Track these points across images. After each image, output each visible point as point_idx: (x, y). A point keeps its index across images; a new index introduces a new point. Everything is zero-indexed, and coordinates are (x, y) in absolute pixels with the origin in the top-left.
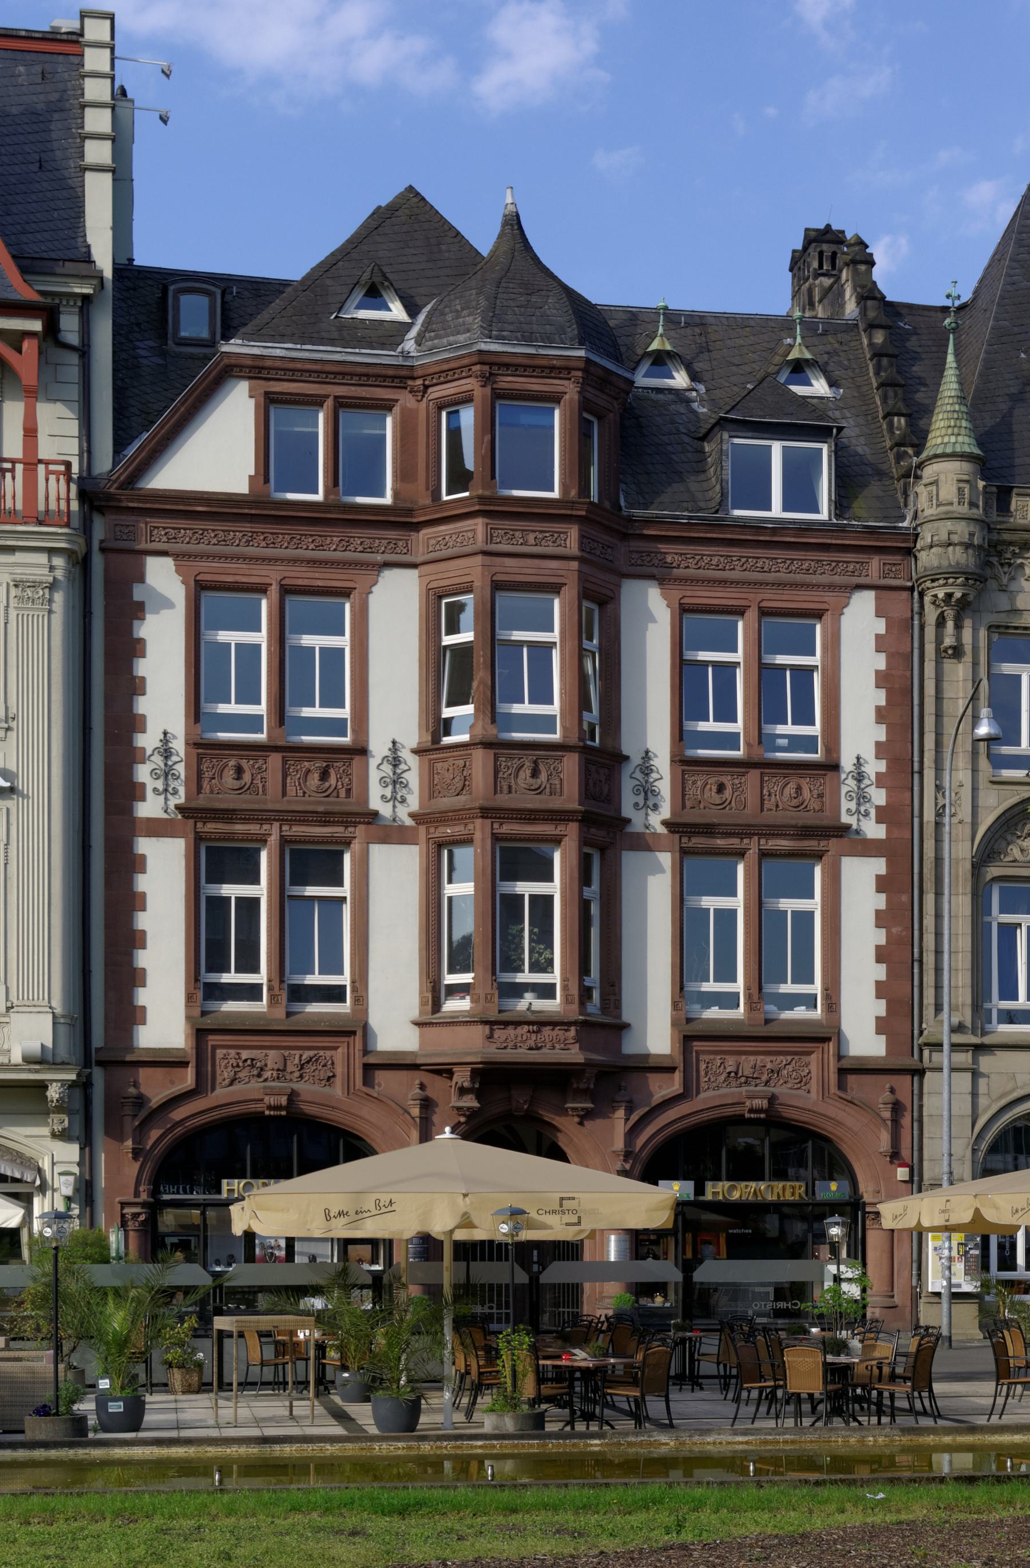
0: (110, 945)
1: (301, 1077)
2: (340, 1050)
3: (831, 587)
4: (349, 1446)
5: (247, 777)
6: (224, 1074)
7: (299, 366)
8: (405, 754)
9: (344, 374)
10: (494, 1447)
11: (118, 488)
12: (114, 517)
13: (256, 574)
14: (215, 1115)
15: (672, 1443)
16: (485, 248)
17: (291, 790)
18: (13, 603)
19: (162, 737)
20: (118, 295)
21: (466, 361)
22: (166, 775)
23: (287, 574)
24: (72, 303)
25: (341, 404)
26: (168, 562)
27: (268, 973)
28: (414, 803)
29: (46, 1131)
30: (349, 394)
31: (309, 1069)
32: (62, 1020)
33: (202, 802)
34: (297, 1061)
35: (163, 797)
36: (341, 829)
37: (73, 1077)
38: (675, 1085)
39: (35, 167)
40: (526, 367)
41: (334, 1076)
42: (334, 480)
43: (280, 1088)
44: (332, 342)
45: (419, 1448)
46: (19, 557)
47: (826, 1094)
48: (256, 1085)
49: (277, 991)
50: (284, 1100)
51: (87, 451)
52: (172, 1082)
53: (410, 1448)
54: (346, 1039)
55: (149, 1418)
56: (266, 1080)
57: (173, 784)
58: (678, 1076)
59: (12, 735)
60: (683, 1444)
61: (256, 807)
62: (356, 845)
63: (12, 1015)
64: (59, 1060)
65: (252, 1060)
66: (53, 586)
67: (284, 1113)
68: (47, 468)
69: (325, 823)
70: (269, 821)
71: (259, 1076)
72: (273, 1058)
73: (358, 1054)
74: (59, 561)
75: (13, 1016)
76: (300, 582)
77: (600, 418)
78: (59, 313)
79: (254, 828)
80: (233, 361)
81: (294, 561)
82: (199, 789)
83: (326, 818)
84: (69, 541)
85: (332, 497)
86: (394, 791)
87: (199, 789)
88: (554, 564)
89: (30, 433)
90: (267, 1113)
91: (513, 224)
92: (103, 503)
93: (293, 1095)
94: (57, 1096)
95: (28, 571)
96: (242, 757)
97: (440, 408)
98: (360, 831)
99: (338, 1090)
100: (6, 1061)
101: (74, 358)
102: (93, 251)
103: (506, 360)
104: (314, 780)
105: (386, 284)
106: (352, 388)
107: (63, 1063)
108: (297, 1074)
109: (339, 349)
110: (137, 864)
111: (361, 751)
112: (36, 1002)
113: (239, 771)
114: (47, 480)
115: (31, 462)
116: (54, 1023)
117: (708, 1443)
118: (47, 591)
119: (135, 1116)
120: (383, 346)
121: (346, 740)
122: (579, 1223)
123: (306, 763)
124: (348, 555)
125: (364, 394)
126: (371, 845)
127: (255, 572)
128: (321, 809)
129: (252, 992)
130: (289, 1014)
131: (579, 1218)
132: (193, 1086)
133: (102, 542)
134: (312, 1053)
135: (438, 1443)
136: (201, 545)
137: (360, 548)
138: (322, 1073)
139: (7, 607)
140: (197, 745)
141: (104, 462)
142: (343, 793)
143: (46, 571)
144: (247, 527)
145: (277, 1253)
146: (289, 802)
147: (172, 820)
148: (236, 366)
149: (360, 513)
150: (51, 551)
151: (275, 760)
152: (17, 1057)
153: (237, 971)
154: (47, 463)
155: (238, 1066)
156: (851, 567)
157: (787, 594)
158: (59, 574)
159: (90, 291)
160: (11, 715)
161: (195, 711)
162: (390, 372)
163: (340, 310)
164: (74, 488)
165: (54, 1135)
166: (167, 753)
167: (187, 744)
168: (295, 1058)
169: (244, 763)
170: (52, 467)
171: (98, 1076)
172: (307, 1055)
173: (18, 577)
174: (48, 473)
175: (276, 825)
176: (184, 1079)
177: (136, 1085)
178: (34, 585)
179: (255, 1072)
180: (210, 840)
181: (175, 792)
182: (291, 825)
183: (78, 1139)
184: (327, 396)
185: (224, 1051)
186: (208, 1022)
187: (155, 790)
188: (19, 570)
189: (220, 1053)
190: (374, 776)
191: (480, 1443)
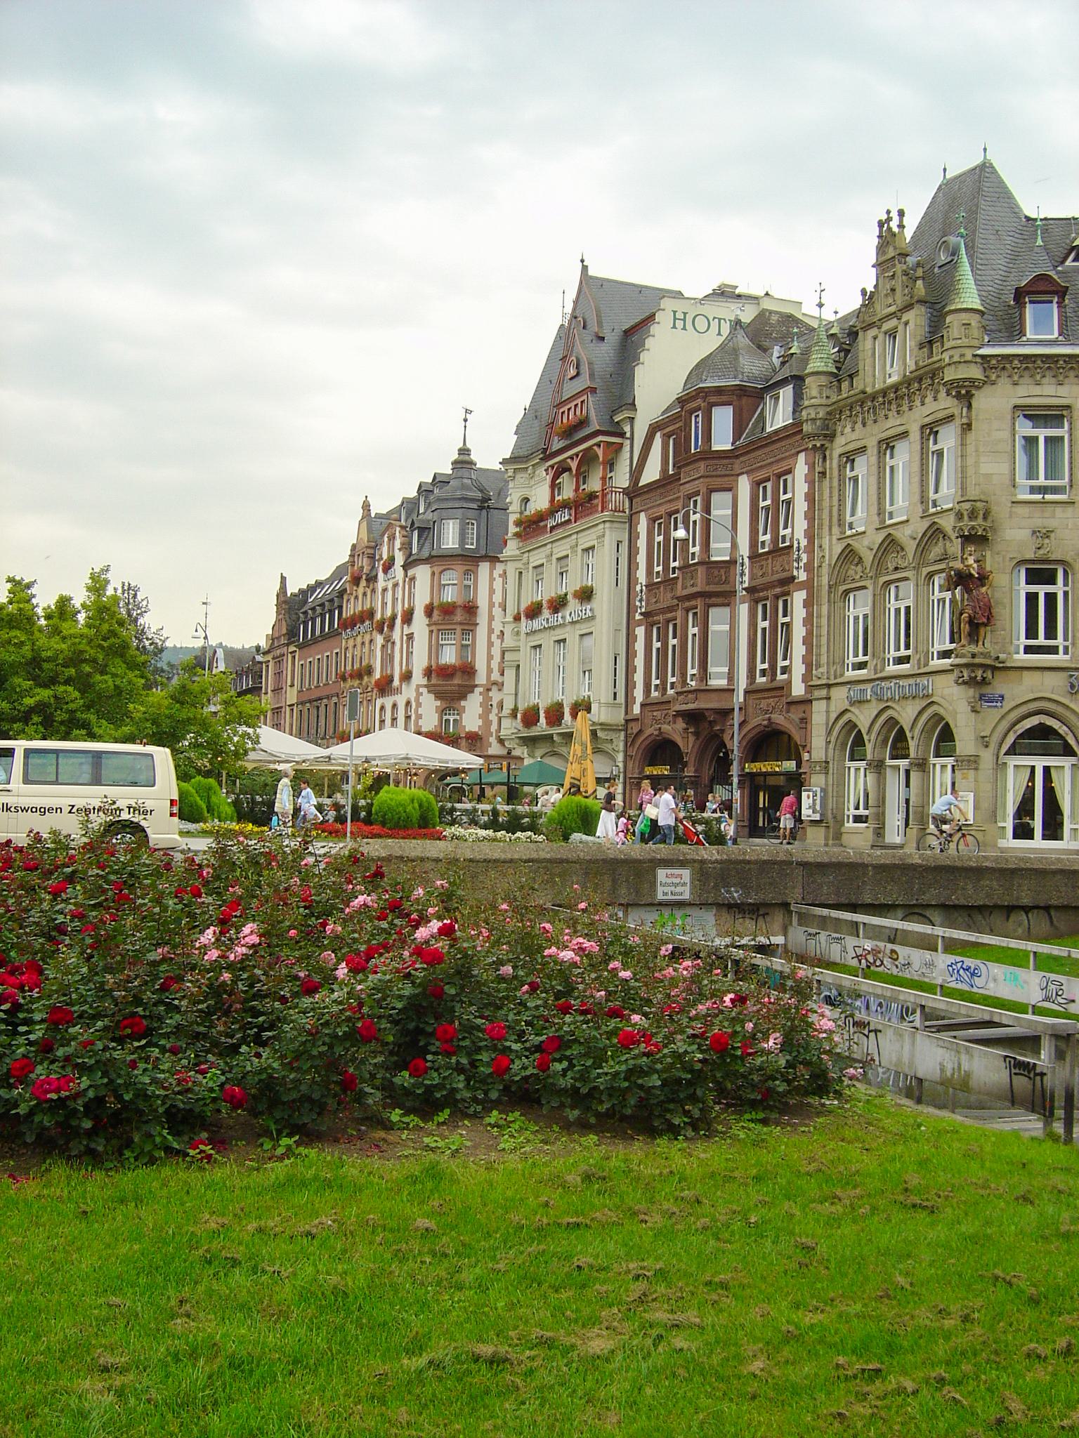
88: (719, 479)
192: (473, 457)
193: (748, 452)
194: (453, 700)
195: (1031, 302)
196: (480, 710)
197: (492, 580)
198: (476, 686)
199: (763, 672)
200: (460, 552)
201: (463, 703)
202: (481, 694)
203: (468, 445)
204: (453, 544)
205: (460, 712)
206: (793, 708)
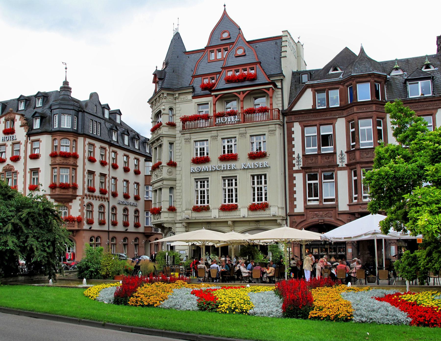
3: (433, 109)
8: (344, 153)
9: (328, 84)
13: (314, 123)
16: (357, 55)
21: (350, 78)
22: (342, 159)
28: (346, 162)
33: (306, 166)
40: (362, 77)
48: (317, 218)
57: (300, 163)
69: (329, 168)
70: (319, 168)
77: (380, 83)
79: (316, 170)
86: (342, 160)
88: (370, 113)
91: (362, 51)
97: (347, 87)
98: (336, 169)
101: (280, 90)
103: (357, 76)
110: (294, 178)
120: (336, 77)
128: (328, 165)
151: (319, 157)
152: (271, 215)
154: (274, 109)
156: (438, 104)
157: (423, 112)
166: (298, 157)
171: (288, 218)
172: (327, 212)
175: (320, 169)
176: (304, 218)
192: (70, 86)
193: (432, 101)
194: (65, 202)
195: (410, 84)
196: (80, 208)
197: (84, 146)
198: (77, 196)
199: (356, 198)
200: (72, 131)
201: (70, 204)
202: (80, 200)
203: (68, 80)
204: (67, 126)
205: (69, 208)
206: (340, 215)
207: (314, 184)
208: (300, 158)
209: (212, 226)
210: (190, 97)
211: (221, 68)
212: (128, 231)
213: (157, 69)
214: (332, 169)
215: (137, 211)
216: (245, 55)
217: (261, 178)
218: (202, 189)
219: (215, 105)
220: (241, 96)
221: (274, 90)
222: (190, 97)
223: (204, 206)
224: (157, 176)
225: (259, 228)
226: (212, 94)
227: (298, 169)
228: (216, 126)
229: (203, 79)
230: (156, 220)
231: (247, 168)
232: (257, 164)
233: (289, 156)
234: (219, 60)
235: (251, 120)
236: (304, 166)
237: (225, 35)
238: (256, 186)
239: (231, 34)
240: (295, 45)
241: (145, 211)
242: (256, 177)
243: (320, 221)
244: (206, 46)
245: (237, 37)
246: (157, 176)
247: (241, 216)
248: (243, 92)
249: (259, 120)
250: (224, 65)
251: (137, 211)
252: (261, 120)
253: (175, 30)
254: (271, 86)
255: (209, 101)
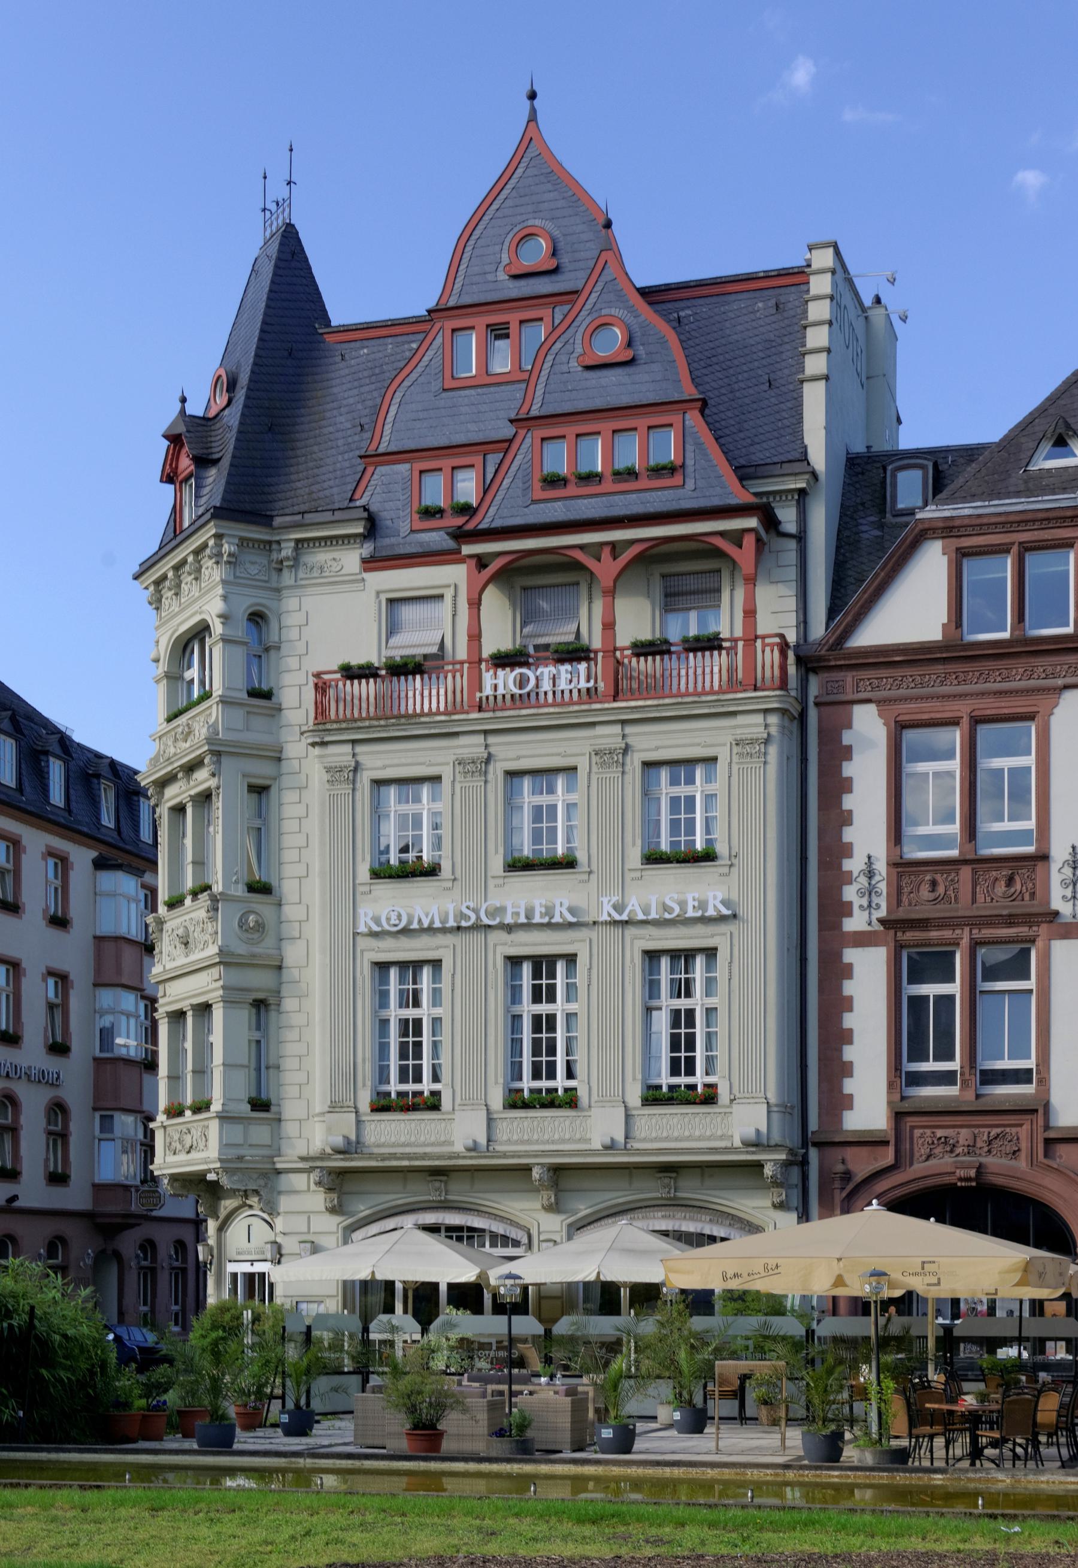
0: (823, 1042)
1: (989, 1151)
2: (1024, 1127)
4: (726, 1471)
5: (941, 890)
6: (922, 1150)
7: (985, 520)
9: (1026, 522)
10: (849, 1477)
11: (828, 650)
12: (826, 675)
13: (949, 709)
14: (914, 1187)
15: (1008, 1481)
17: (980, 898)
18: (735, 759)
19: (866, 860)
20: (848, 481)
23: (976, 707)
24: (790, 497)
25: (1027, 548)
26: (872, 708)
27: (962, 1061)
29: (768, 1203)
30: (1033, 539)
31: (996, 1144)
32: (775, 1109)
33: (902, 914)
34: (985, 1138)
35: (867, 912)
36: (1026, 929)
37: (784, 1157)
38: (888, 1157)
39: (766, 387)
41: (1019, 1150)
42: (1020, 616)
43: (970, 1162)
44: (1018, 494)
45: (784, 1475)
46: (741, 720)
47: (1035, 1162)
48: (949, 1159)
49: (967, 1077)
50: (972, 1173)
51: (804, 623)
52: (876, 1159)
53: (777, 1475)
54: (1029, 1117)
55: (638, 1445)
56: (958, 1155)
57: (875, 900)
58: (891, 1149)
59: (735, 870)
60: (1019, 1481)
61: (947, 915)
62: (1040, 943)
63: (734, 1106)
64: (772, 1143)
65: (946, 1138)
66: (767, 741)
67: (974, 1184)
68: (763, 642)
69: (1011, 925)
70: (960, 926)
71: (952, 1151)
72: (964, 1135)
73: (1041, 1130)
74: (773, 719)
75: (735, 1107)
76: (988, 712)
78: (773, 509)
79: (947, 934)
80: (926, 526)
81: (983, 694)
82: (899, 903)
83: (1011, 920)
84: (780, 702)
85: (1017, 633)
87: (899, 903)
89: (750, 613)
90: (959, 1184)
92: (816, 665)
93: (980, 1169)
94: (771, 1173)
95: (746, 731)
96: (936, 872)
98: (1043, 930)
99: (1022, 1163)
100: (729, 1145)
101: (792, 544)
102: (810, 451)
104: (1001, 888)
105: (1070, 433)
106: (1036, 533)
107: (776, 1145)
108: (986, 1149)
109: (1023, 500)
110: (847, 971)
111: (1043, 857)
112: (754, 1095)
113: (934, 884)
114: (763, 652)
115: (751, 639)
116: (769, 1112)
117: (1042, 1482)
118: (762, 746)
119: (843, 1189)
121: (1030, 849)
122: (939, 1284)
123: (994, 873)
124: (1032, 683)
125: (1046, 537)
126: (1053, 943)
127: (947, 708)
128: (1005, 912)
129: (948, 1078)
130: (978, 1096)
131: (939, 1279)
132: (893, 1162)
133: (816, 697)
134: (999, 1130)
135: (801, 1472)
136: (901, 690)
137: (1043, 675)
138: (1008, 1148)
139: (730, 763)
140: (896, 865)
141: (818, 629)
142: (1027, 897)
143: (762, 729)
144: (940, 668)
145: (979, 1308)
146: (977, 908)
147: (875, 932)
148: (929, 529)
149: (1038, 644)
150: (766, 711)
151: (966, 872)
152: (737, 1143)
153: (935, 1059)
154: (763, 637)
155: (933, 1143)
158: (774, 730)
159: (804, 485)
160: (734, 854)
161: (896, 833)
162: (1069, 513)
163: (1027, 466)
164: (791, 655)
165: (775, 1206)
166: (870, 874)
167: (888, 864)
168: (984, 1134)
169: (938, 877)
170: (768, 641)
171: (813, 1154)
172: (995, 1131)
173: (738, 737)
174: (764, 646)
175: (967, 929)
177: (843, 1162)
178: (752, 742)
179: (948, 1149)
180: (909, 946)
181: (878, 906)
182: (980, 929)
183: (797, 1209)
184: (1013, 544)
185: (921, 1131)
186: (906, 1106)
187: (861, 906)
188: (739, 731)
189: (917, 1132)
190: (1055, 879)
191: (836, 1473)
207: (939, 999)
208: (877, 878)
209: (454, 1186)
210: (351, 559)
211: (511, 421)
212: (16, 1204)
213: (183, 411)
214: (1023, 931)
215: (58, 1109)
216: (631, 362)
217: (552, 975)
218: (543, 1008)
219: (475, 604)
220: (606, 569)
221: (765, 544)
222: (351, 559)
223: (549, 1091)
224: (186, 944)
225: (446, 1201)
226: (467, 550)
227: (865, 927)
228: (480, 709)
229: (416, 474)
230: (182, 1157)
231: (625, 917)
232: (473, 910)
233: (822, 865)
234: (502, 381)
235: (653, 688)
236: (893, 917)
237: (536, 253)
238: (395, 1013)
239: (561, 245)
240: (862, 319)
241: (95, 1109)
242: (527, 969)
243: (961, 1173)
244: (431, 304)
245: (591, 263)
246: (186, 944)
247: (597, 1145)
248: (615, 547)
249: (691, 689)
250: (525, 409)
251: (58, 1109)
252: (699, 689)
253: (273, 207)
254: (752, 522)
255: (449, 586)
